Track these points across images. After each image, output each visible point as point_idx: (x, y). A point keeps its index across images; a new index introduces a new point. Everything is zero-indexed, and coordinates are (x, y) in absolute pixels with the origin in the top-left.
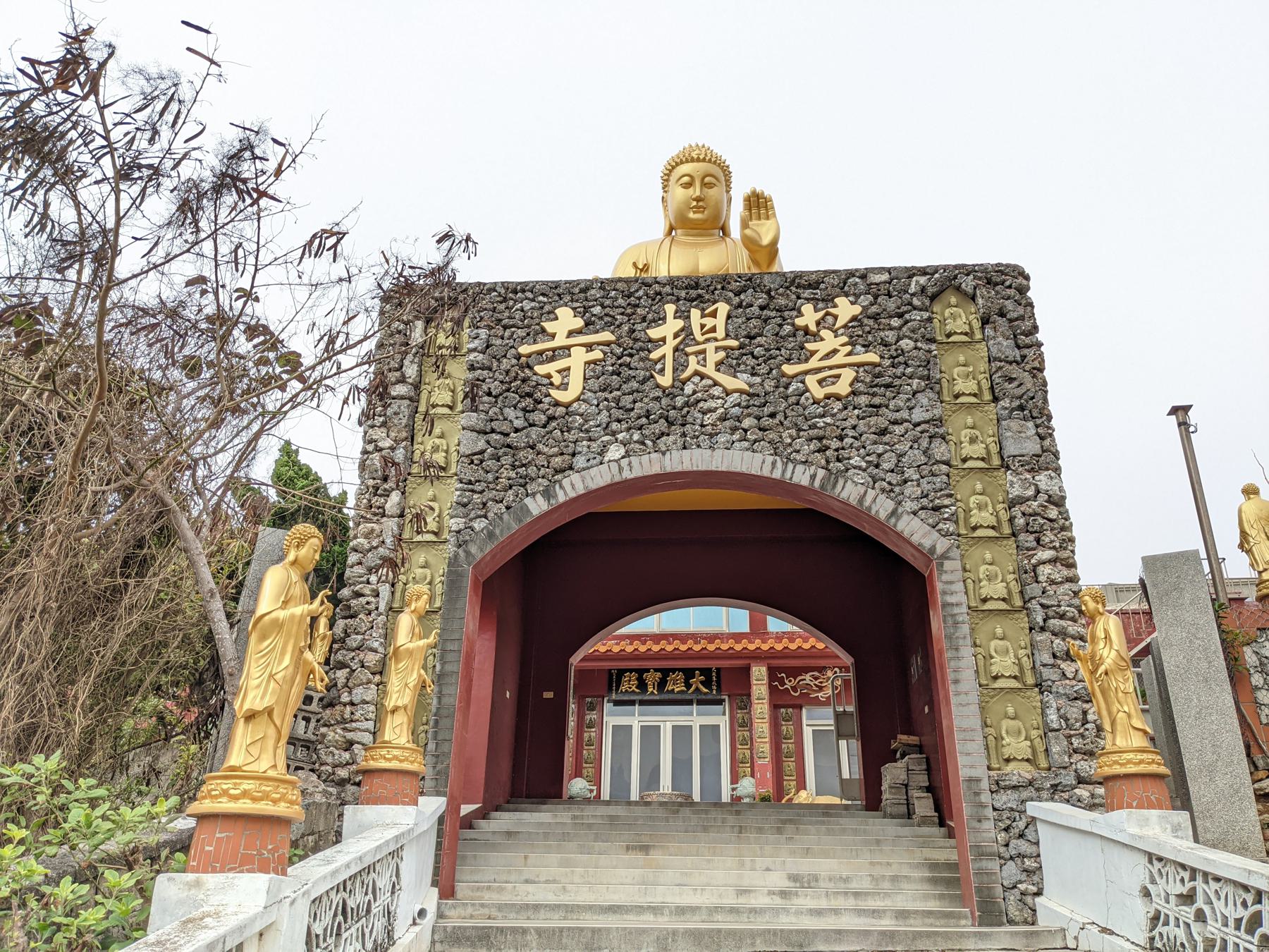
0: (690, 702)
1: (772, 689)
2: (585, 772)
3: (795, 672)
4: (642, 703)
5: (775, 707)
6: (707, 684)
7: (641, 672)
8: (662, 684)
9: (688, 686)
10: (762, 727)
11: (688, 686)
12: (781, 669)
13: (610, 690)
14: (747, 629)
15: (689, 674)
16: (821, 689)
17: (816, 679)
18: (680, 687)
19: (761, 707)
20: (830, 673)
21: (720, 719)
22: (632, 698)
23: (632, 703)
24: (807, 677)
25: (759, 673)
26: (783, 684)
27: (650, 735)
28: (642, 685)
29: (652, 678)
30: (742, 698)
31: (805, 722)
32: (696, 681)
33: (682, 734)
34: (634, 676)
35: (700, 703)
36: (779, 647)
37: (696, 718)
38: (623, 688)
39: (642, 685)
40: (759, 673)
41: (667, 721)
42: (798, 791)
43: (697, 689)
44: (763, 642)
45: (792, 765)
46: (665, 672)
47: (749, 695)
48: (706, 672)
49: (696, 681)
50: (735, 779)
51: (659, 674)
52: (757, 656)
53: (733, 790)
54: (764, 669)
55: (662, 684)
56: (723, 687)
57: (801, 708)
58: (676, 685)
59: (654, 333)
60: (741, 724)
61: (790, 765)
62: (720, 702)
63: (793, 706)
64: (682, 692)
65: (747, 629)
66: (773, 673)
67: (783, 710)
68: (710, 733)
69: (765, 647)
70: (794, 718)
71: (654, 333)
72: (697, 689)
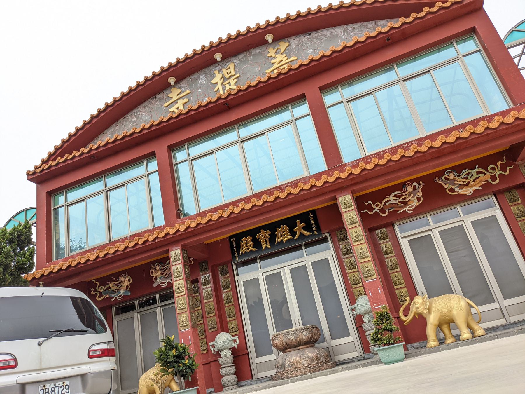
0: (299, 248)
1: (364, 218)
2: (230, 325)
3: (379, 196)
4: (262, 258)
5: (370, 230)
6: (308, 228)
7: (253, 233)
8: (272, 239)
9: (293, 234)
10: (361, 247)
11: (293, 234)
12: (367, 197)
13: (233, 255)
14: (325, 168)
15: (290, 223)
16: (406, 204)
17: (399, 197)
18: (287, 237)
19: (355, 229)
20: (410, 189)
21: (326, 252)
22: (253, 256)
23: (254, 261)
24: (392, 198)
25: (346, 201)
26: (372, 209)
27: (274, 280)
28: (257, 244)
29: (263, 236)
30: (339, 231)
31: (399, 235)
32: (300, 226)
33: (299, 274)
34: (249, 238)
35: (307, 245)
36: (357, 171)
37: (307, 258)
38: (243, 251)
39: (257, 244)
40: (346, 201)
41: (284, 266)
42: (412, 299)
43: (301, 234)
44: (342, 172)
45: (399, 275)
46: (272, 227)
47: (344, 228)
48: (304, 217)
49: (300, 226)
50: (352, 300)
51: (268, 232)
52: (339, 187)
53: (353, 310)
54: (349, 197)
55: (272, 239)
56: (322, 227)
57: (393, 225)
58: (283, 236)
59: (214, 81)
60: (344, 253)
61: (397, 275)
62: (325, 240)
63: (386, 226)
64: (289, 240)
65: (325, 168)
66: (360, 203)
67: (378, 232)
68: (321, 267)
69: (344, 175)
70: (390, 235)
71: (214, 81)
72: (301, 234)
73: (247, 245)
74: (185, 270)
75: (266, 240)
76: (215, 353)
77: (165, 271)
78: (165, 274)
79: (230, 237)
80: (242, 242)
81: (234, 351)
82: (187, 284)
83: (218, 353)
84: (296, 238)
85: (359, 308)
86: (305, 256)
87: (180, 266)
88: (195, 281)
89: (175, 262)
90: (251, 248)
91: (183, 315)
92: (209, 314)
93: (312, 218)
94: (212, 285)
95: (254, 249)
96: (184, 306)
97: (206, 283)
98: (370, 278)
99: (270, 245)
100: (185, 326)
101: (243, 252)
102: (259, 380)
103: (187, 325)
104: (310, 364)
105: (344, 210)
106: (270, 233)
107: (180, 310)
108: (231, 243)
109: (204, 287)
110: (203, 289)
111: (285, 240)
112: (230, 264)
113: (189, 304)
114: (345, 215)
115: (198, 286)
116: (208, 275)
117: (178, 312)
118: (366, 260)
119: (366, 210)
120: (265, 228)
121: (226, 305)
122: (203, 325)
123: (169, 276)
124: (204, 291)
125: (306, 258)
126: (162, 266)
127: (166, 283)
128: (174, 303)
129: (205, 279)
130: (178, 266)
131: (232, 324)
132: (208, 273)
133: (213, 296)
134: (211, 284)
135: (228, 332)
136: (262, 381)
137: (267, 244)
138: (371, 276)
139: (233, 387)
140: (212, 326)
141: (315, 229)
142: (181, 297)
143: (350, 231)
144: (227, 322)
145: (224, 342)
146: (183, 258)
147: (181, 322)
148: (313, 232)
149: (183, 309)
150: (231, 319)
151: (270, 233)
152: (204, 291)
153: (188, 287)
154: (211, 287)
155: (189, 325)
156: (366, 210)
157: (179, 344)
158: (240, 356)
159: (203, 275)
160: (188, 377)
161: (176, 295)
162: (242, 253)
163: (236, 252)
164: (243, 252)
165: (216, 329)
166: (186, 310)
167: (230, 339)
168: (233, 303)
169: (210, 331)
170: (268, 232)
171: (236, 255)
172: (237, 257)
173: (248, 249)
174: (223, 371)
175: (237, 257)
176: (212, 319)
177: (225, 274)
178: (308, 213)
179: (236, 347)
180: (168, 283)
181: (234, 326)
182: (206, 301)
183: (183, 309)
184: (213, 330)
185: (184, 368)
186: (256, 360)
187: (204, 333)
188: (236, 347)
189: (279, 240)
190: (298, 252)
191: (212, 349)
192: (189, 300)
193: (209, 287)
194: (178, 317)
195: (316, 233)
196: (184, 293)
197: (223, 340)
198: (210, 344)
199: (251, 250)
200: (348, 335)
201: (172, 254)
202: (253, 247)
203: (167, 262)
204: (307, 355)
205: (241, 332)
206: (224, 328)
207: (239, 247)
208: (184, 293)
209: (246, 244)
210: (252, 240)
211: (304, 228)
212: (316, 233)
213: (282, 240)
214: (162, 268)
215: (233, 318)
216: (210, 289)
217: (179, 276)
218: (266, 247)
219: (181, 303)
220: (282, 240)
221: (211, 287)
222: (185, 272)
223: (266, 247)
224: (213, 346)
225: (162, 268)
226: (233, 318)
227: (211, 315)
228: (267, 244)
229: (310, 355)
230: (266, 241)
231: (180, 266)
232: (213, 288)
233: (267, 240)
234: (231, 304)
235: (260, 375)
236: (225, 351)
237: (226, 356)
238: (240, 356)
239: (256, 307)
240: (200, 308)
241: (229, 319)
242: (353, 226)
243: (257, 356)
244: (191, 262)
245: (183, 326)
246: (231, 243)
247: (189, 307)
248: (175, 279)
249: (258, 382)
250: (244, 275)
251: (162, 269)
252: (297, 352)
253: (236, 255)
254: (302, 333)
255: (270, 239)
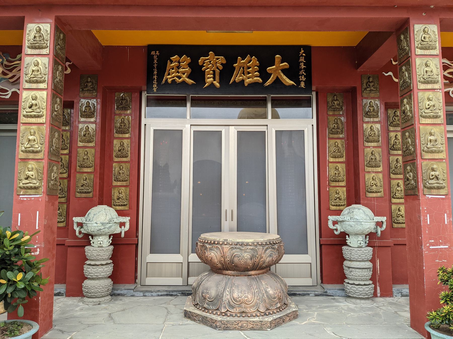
2: (115, 193)
4: (196, 102)
6: (291, 73)
7: (195, 52)
8: (226, 73)
9: (265, 75)
11: (265, 75)
28: (197, 73)
29: (212, 64)
33: (251, 143)
34: (186, 60)
37: (277, 123)
38: (168, 78)
39: (197, 73)
41: (229, 125)
43: (278, 81)
46: (232, 53)
48: (289, 53)
51: (222, 59)
58: (247, 72)
62: (307, 103)
64: (254, 85)
68: (290, 141)
72: (278, 81)
73: (178, 71)
74: (54, 74)
75: (214, 71)
76: (81, 236)
77: (11, 71)
78: (10, 75)
79: (151, 47)
80: (172, 62)
81: (116, 239)
82: (53, 102)
83: (87, 238)
84: (268, 83)
85: (352, 223)
86: (188, 117)
87: (45, 60)
88: (68, 105)
89: (35, 48)
90: (184, 77)
91: (32, 164)
92: (82, 166)
93: (302, 59)
94: (98, 121)
95: (190, 81)
96: (37, 147)
97: (88, 114)
98: (434, 191)
99: (219, 83)
100: (31, 188)
101: (169, 81)
102: (147, 291)
103: (35, 188)
104: (268, 309)
105: (419, 52)
106: (224, 62)
107: (26, 152)
108: (150, 59)
109: (82, 119)
110: (79, 122)
111: (248, 81)
112: (137, 95)
113: (51, 145)
114: (418, 61)
115: (70, 115)
116: (94, 101)
117: (22, 155)
118: (436, 156)
119: (390, 73)
120: (219, 50)
121: (116, 159)
122: (66, 181)
123: (16, 82)
124: (81, 126)
125: (269, 121)
126: (7, 61)
127: (10, 93)
128: (15, 131)
129: (88, 106)
130: (39, 59)
131: (120, 192)
132: (96, 97)
133: (97, 139)
134: (97, 118)
135: (110, 205)
136: (154, 294)
137: (214, 78)
138: (439, 188)
139: (103, 299)
140: (85, 189)
141: (303, 78)
142: (34, 127)
143: (420, 94)
144: (111, 187)
145: (103, 224)
146: (55, 46)
147: (23, 177)
148: (298, 82)
149: (33, 152)
150: (119, 183)
151: (224, 62)
152: (81, 126)
153: (53, 111)
154: (95, 122)
155: (42, 189)
156: (390, 73)
157: (8, 233)
158: (124, 249)
159: (84, 98)
160: (17, 306)
161: (22, 119)
162: (167, 80)
163: (155, 77)
164: (169, 81)
165: (91, 195)
166: (40, 156)
167: (116, 220)
168: (128, 159)
169: (78, 195)
170: (222, 59)
171: (155, 82)
172: (155, 86)
173: (179, 77)
174: (88, 270)
175: (155, 86)
176: (86, 178)
177: (125, 109)
178: (298, 48)
179: (123, 235)
180: (13, 93)
181: (123, 195)
182: (80, 144)
183: (33, 152)
184: (83, 195)
185: (9, 291)
186: (148, 257)
187: (68, 200)
188: (123, 235)
189: (238, 78)
190: (259, 110)
191: (77, 229)
192: (52, 136)
193: (376, 122)
194: (19, 166)
195: (303, 85)
196: (42, 120)
197: (102, 220)
198: (76, 219)
199: (184, 82)
200: (305, 251)
201: (31, 29)
202: (189, 77)
203: (18, 56)
204: (266, 292)
205: (132, 209)
206: (105, 199)
207: (162, 70)
208: (42, 120)
209: (178, 67)
210: (190, 65)
211: (284, 71)
212: (303, 85)
213: (243, 81)
214: (5, 63)
215: (124, 183)
216: (92, 126)
217: (37, 82)
218: (212, 84)
219: (31, 138)
220: (243, 81)
221: (95, 122)
222: (54, 77)
223: (212, 84)
224: (80, 225)
225: (5, 63)
226: (124, 183)
227: (86, 170)
228: (215, 80)
229: (271, 292)
230: (214, 74)
231: (45, 60)
232: (99, 126)
233: (217, 71)
234: (124, 159)
235: (149, 281)
236: (100, 239)
237: (101, 248)
238: (124, 249)
239: (166, 174)
240: (66, 152)
241: (115, 183)
242: (429, 86)
243: (152, 251)
244: (66, 69)
245: (28, 188)
246: (150, 59)
247: (49, 151)
248: (27, 85)
249: (147, 294)
250: (155, 121)
251: (6, 66)
252: (245, 279)
253: (155, 82)
254: (266, 250)
255: (221, 72)
